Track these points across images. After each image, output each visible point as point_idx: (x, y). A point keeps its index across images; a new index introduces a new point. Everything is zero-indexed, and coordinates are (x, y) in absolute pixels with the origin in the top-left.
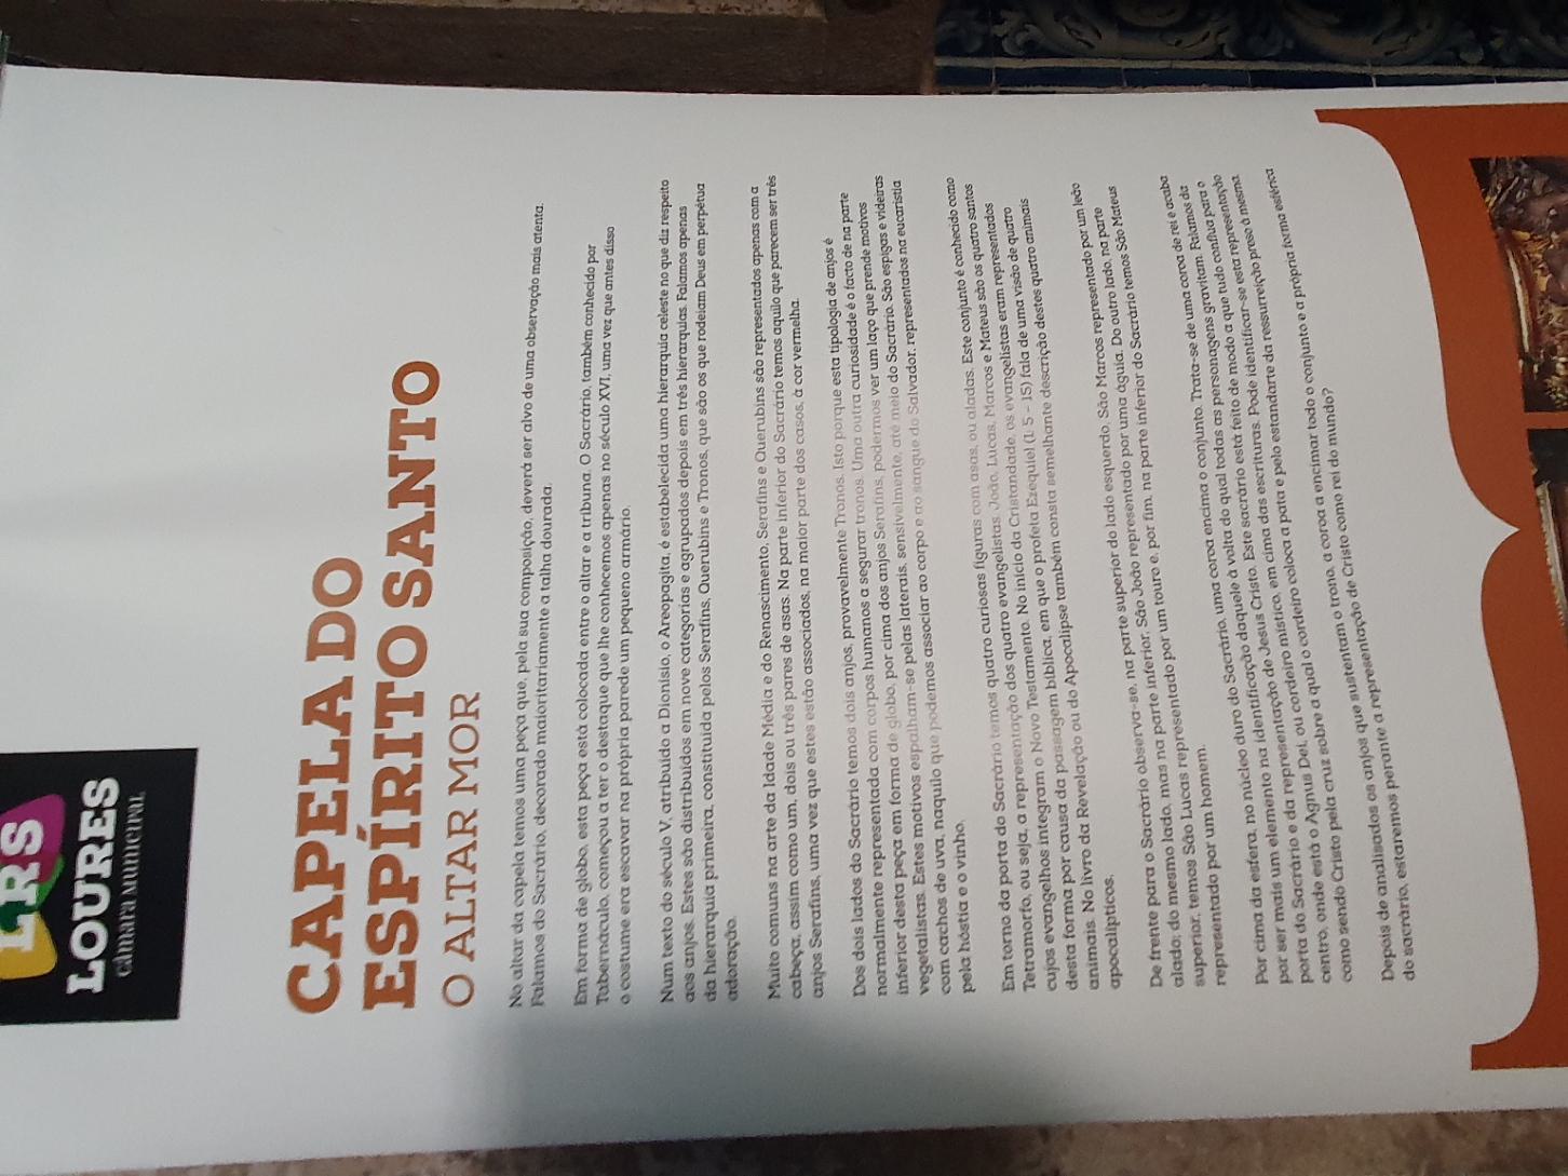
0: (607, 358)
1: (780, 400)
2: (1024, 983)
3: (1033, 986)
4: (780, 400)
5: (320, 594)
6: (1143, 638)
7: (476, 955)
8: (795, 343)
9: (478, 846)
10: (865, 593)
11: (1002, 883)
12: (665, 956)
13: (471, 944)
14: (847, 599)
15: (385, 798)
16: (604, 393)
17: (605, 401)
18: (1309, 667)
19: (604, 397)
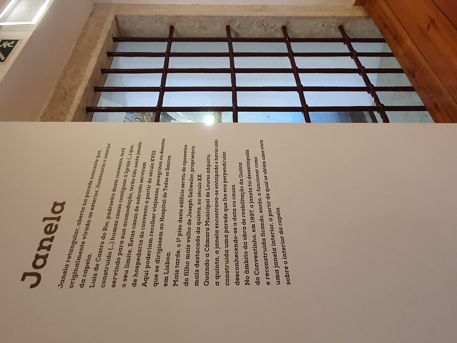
0: (278, 278)
1: (193, 151)
2: (164, 189)
3: (167, 190)
4: (193, 151)
5: (149, 262)
6: (271, 226)
7: (147, 286)
8: (224, 177)
9: (54, 240)
10: (235, 224)
11: (225, 232)
12: (176, 267)
13: (146, 284)
14: (218, 205)
15: (46, 249)
16: (152, 159)
17: (152, 162)
18: (267, 184)
19: (152, 160)
